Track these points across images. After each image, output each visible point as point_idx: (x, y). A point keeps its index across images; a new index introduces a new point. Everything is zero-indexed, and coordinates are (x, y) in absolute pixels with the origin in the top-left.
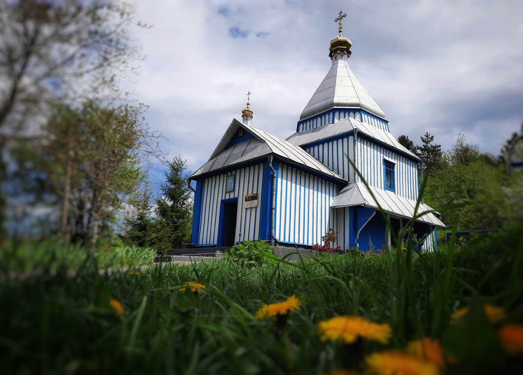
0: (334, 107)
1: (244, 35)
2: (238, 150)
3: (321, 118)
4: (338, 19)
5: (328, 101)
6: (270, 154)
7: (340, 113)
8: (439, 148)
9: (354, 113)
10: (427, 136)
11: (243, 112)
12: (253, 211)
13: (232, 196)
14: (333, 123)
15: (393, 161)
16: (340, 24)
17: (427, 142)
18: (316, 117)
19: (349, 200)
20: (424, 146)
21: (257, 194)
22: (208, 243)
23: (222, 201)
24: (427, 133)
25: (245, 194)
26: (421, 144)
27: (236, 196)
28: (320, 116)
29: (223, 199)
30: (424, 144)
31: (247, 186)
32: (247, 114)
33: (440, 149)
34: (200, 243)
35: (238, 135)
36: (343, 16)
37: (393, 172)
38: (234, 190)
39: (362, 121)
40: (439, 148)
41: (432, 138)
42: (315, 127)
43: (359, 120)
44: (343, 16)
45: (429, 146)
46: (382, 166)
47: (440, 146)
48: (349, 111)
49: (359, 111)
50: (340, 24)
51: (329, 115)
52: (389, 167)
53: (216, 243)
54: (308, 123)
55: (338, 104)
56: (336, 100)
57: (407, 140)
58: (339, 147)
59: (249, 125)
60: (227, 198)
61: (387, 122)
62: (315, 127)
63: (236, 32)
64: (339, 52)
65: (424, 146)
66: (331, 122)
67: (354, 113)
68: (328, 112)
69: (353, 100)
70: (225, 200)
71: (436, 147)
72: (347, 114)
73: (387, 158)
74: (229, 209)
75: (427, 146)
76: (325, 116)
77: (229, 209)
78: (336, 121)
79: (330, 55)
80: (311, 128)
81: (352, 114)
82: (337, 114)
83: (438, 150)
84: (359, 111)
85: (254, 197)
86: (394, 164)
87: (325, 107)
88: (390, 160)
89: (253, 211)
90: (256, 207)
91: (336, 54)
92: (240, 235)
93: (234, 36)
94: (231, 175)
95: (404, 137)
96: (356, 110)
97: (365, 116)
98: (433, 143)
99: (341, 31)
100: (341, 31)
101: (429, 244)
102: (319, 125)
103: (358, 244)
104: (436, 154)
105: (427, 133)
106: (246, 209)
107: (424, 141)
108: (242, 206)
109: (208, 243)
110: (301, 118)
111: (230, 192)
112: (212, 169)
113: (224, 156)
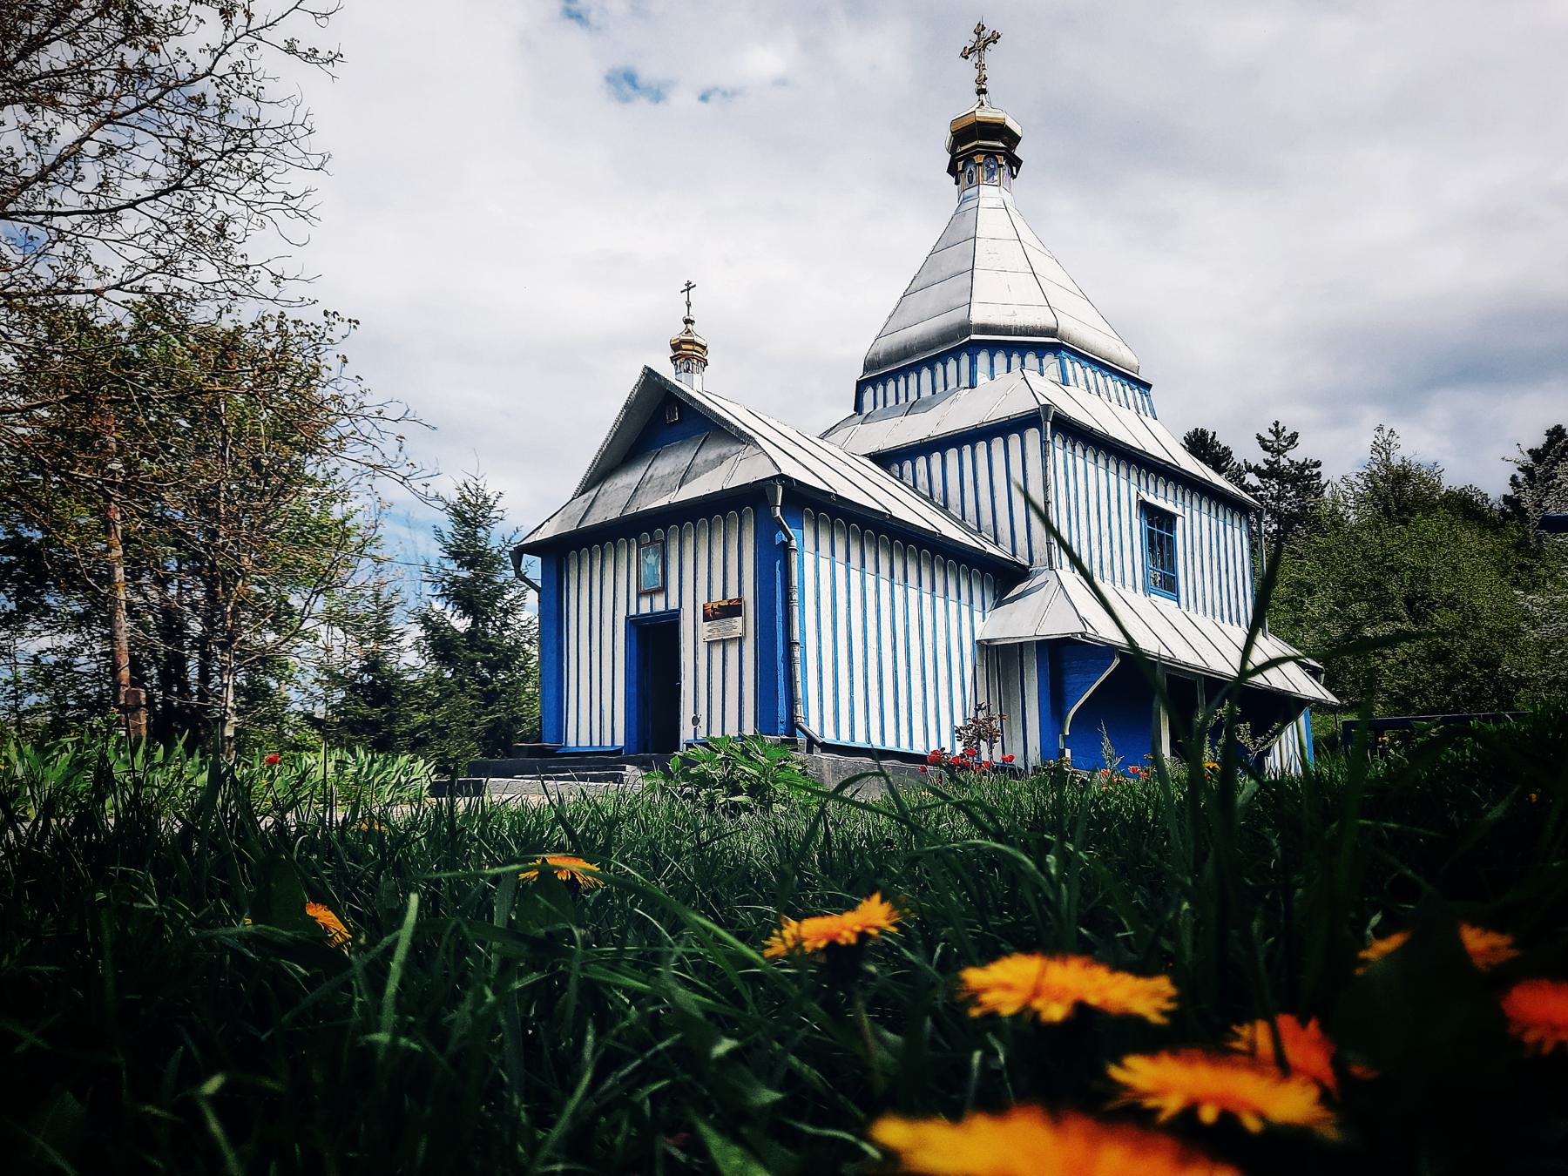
2: (666, 466)
4: (972, 50)
5: (956, 317)
6: (773, 478)
7: (992, 356)
8: (1315, 471)
10: (1277, 434)
11: (675, 347)
12: (733, 651)
13: (659, 604)
14: (972, 386)
16: (980, 66)
17: (1279, 452)
18: (916, 368)
21: (740, 600)
22: (596, 743)
24: (1277, 424)
26: (1259, 457)
27: (673, 605)
28: (930, 363)
29: (633, 612)
30: (1268, 455)
31: (706, 574)
32: (687, 352)
33: (1318, 475)
34: (572, 742)
35: (661, 417)
36: (987, 41)
37: (1171, 541)
38: (664, 589)
40: (1315, 471)
41: (1295, 436)
42: (913, 397)
44: (987, 41)
47: (1317, 464)
49: (1056, 349)
50: (980, 66)
51: (958, 360)
52: (1159, 523)
53: (620, 742)
55: (985, 329)
56: (978, 317)
59: (695, 386)
61: (1148, 386)
62: (913, 397)
64: (979, 159)
65: (1266, 461)
68: (955, 353)
71: (1302, 467)
72: (1015, 359)
75: (1277, 462)
76: (945, 365)
78: (982, 378)
79: (952, 170)
80: (902, 401)
81: (1031, 359)
82: (983, 358)
83: (1311, 477)
85: (732, 610)
88: (1160, 503)
89: (733, 651)
90: (740, 640)
92: (695, 721)
94: (653, 541)
95: (1204, 433)
97: (1074, 368)
98: (1296, 455)
99: (984, 92)
100: (984, 92)
101: (1286, 752)
104: (1307, 488)
105: (1277, 424)
107: (1266, 448)
108: (693, 635)
109: (596, 743)
111: (651, 593)
112: (591, 521)
113: (625, 482)
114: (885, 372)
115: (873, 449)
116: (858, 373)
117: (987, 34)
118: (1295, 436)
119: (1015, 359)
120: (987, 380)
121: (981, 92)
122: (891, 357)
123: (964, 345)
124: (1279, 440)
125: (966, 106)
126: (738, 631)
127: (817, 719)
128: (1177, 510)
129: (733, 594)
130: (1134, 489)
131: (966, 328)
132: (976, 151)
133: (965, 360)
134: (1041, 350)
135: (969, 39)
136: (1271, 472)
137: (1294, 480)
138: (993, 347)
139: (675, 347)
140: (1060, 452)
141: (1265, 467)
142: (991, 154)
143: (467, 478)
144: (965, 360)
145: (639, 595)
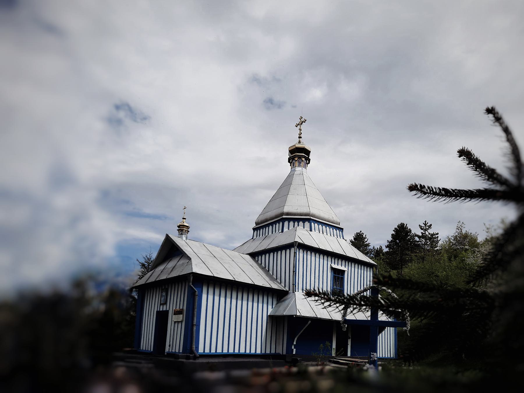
0: (284, 217)
1: (280, 106)
2: (171, 264)
3: (273, 226)
4: (298, 125)
8: (436, 236)
9: (304, 223)
10: (425, 225)
12: (180, 325)
13: (165, 309)
14: (282, 231)
15: (343, 268)
16: (300, 130)
17: (426, 230)
19: (284, 311)
20: (422, 233)
23: (157, 311)
24: (425, 222)
25: (174, 308)
26: (419, 232)
27: (168, 309)
30: (423, 231)
31: (176, 301)
33: (438, 237)
36: (303, 122)
39: (311, 230)
40: (436, 236)
41: (431, 225)
42: (267, 234)
43: (309, 229)
44: (303, 122)
45: (427, 233)
46: (329, 274)
47: (437, 234)
48: (298, 220)
49: (309, 220)
50: (300, 130)
51: (279, 224)
54: (271, 227)
55: (288, 214)
56: (286, 210)
57: (406, 228)
58: (283, 257)
59: (181, 242)
60: (161, 310)
61: (342, 229)
63: (270, 103)
64: (296, 159)
65: (422, 233)
66: (280, 231)
67: (304, 223)
68: (278, 221)
69: (304, 210)
70: (160, 311)
71: (432, 235)
72: (296, 223)
73: (335, 266)
74: (162, 318)
75: (425, 233)
76: (276, 225)
77: (162, 318)
78: (286, 229)
79: (289, 162)
81: (301, 223)
82: (286, 223)
83: (435, 238)
84: (309, 220)
86: (343, 272)
87: (277, 217)
88: (339, 267)
89: (180, 325)
91: (294, 161)
92: (170, 346)
93: (268, 108)
95: (403, 224)
96: (306, 219)
97: (315, 226)
98: (431, 231)
99: (301, 137)
100: (301, 137)
102: (270, 233)
103: (295, 350)
104: (433, 241)
105: (425, 222)
106: (175, 322)
107: (422, 229)
108: (172, 318)
110: (257, 224)
111: (163, 304)
112: (148, 282)
114: (261, 226)
115: (251, 251)
116: (254, 225)
117: (303, 120)
118: (431, 225)
119: (296, 223)
120: (287, 230)
121: (300, 137)
122: (262, 222)
123: (282, 219)
124: (426, 226)
125: (294, 142)
126: (180, 320)
127: (203, 346)
128: (346, 269)
129: (181, 308)
130: (329, 263)
131: (282, 214)
132: (295, 157)
133: (281, 224)
134: (304, 220)
135: (298, 121)
136: (423, 236)
137: (430, 239)
138: (289, 220)
139: (179, 227)
140: (301, 254)
141: (421, 235)
142: (300, 157)
143: (147, 254)
144: (281, 224)
145: (161, 304)
